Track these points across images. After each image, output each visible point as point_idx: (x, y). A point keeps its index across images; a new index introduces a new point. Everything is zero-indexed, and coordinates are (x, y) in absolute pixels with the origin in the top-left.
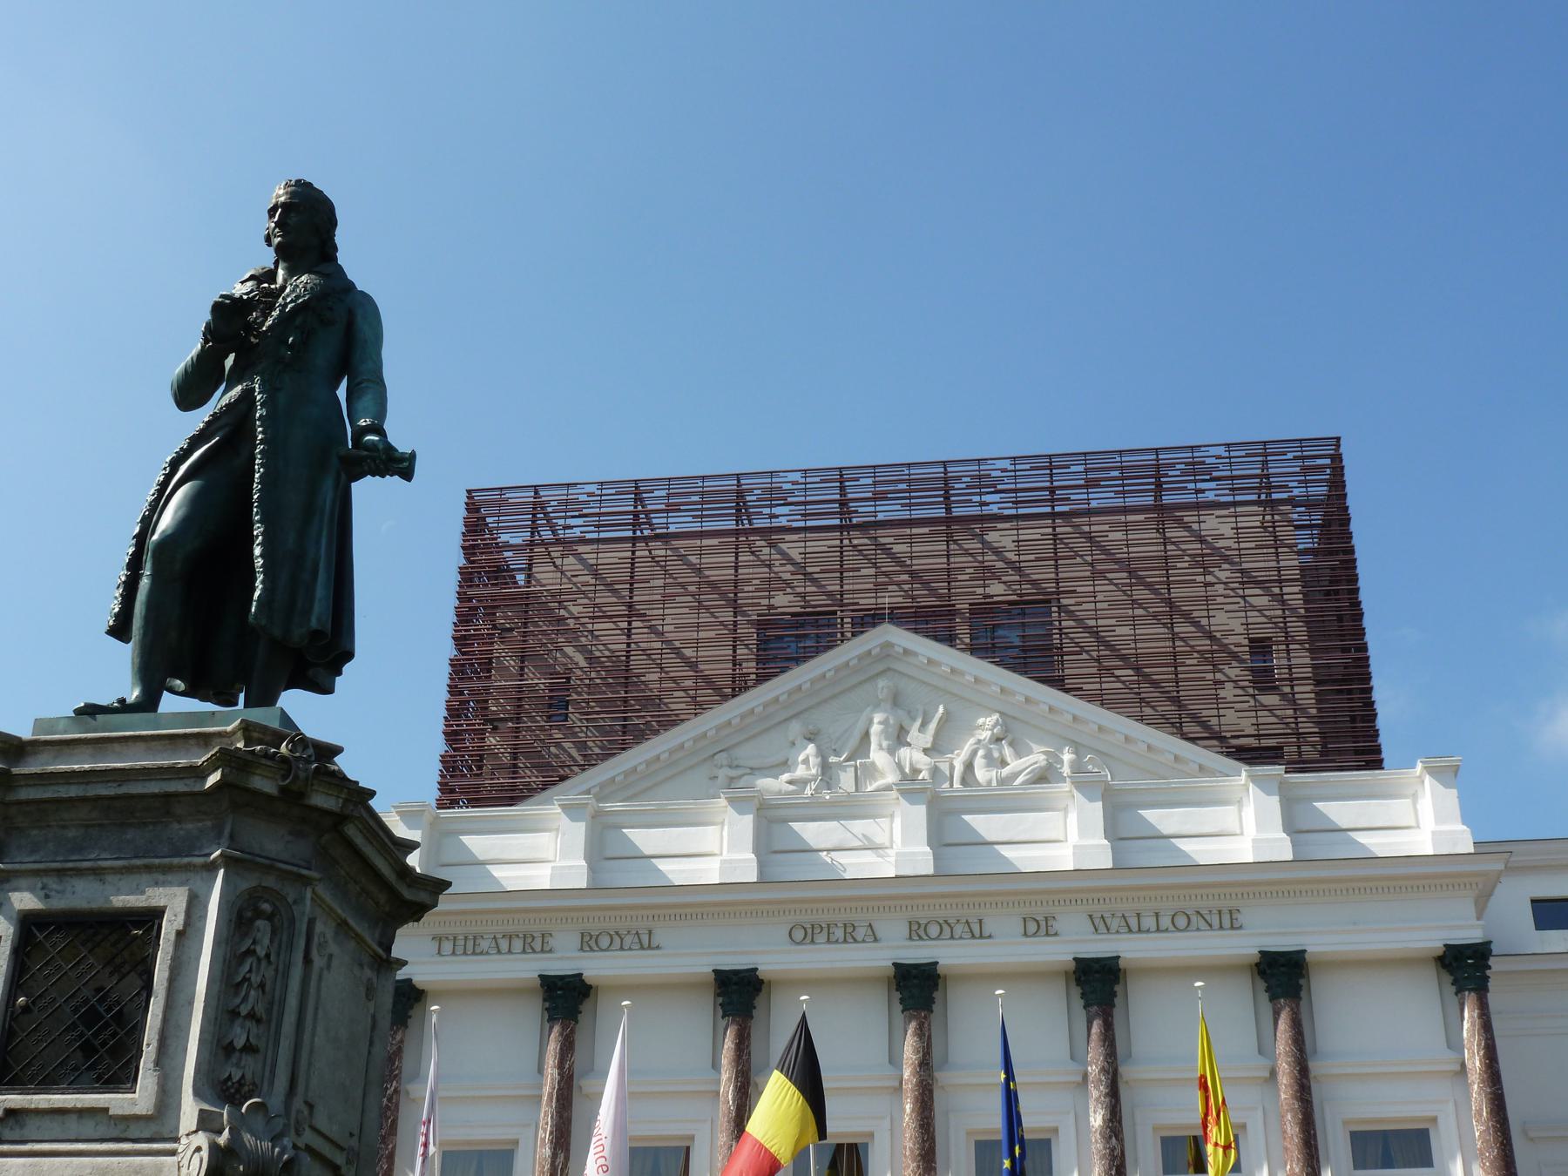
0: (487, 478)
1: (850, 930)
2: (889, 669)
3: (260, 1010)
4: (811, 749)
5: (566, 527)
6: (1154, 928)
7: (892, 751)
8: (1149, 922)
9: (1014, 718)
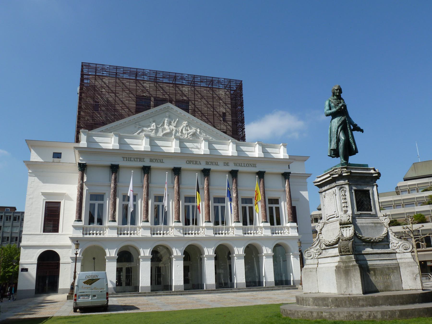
1: (196, 162)
2: (168, 111)
4: (154, 124)
6: (243, 166)
7: (169, 126)
8: (243, 165)
9: (190, 123)
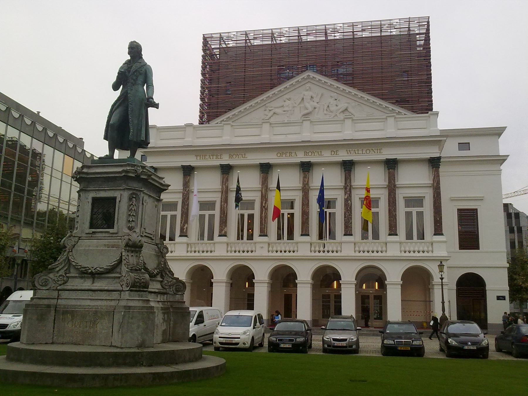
0: (208, 31)
3: (134, 214)
5: (228, 44)
